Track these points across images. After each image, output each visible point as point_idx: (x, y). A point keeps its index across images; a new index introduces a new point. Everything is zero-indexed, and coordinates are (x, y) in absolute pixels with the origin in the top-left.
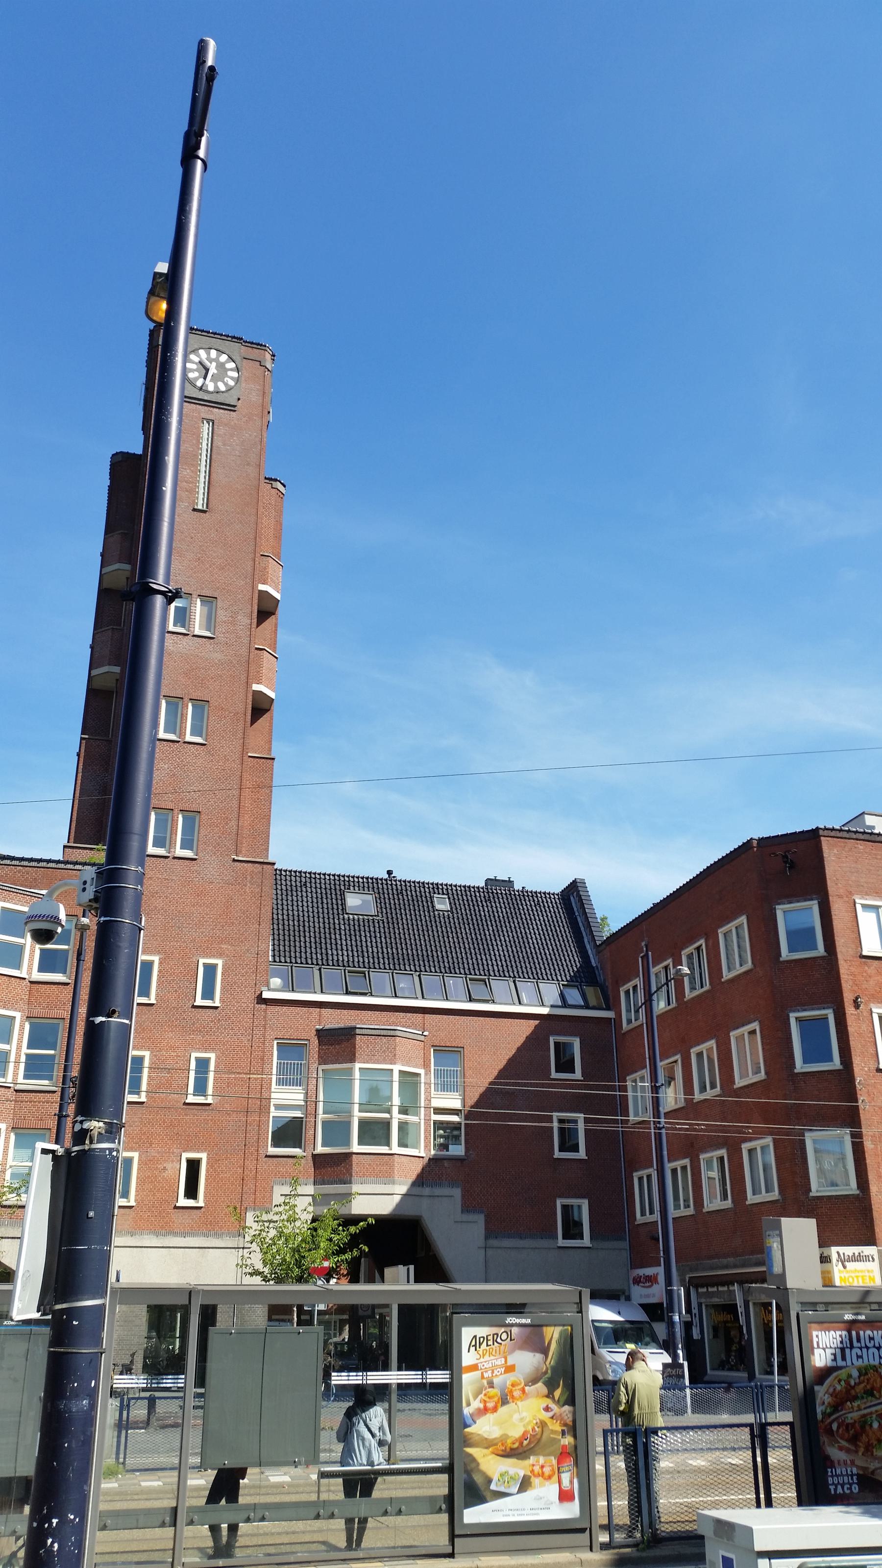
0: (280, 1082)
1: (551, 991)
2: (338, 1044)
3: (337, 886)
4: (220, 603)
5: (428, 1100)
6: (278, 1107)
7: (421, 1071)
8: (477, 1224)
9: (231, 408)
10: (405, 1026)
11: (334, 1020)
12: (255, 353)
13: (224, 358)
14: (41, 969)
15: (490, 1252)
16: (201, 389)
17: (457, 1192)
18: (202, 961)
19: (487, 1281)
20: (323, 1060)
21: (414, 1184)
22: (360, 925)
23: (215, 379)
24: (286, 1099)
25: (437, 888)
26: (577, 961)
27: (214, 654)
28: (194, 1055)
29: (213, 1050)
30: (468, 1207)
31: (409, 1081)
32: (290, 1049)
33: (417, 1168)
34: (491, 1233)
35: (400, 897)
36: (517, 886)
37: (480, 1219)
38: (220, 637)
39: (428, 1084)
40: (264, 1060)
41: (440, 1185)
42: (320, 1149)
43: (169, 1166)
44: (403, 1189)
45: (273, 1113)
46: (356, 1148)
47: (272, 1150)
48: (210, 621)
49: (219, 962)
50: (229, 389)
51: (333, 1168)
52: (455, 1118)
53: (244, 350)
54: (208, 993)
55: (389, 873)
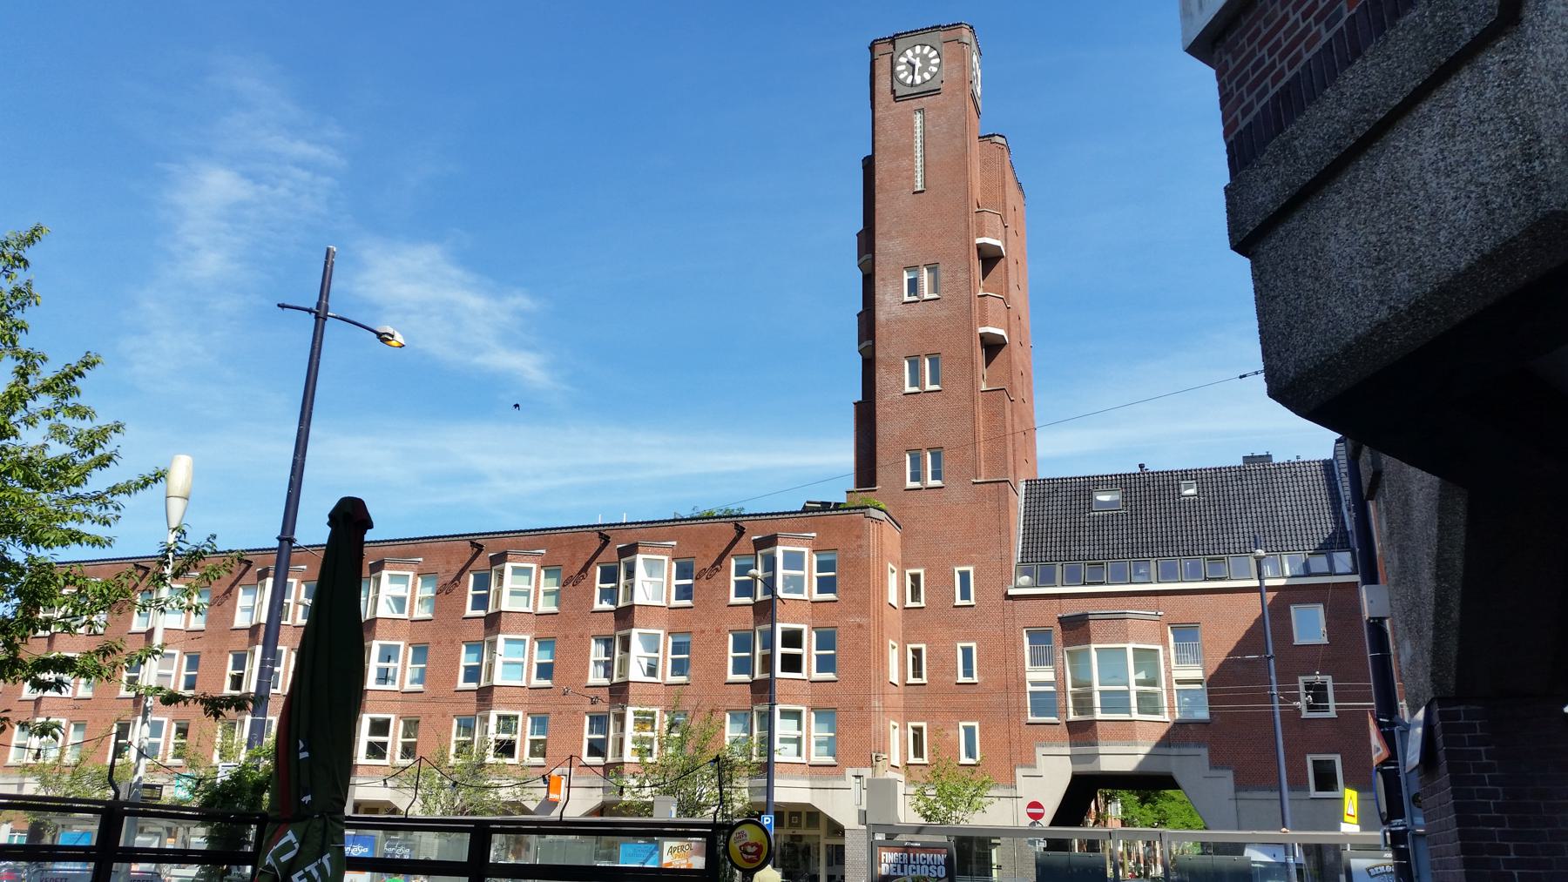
0: (1033, 663)
1: (265, 808)
2: (1076, 628)
3: (1085, 487)
4: (941, 267)
5: (1169, 672)
6: (1033, 684)
7: (1160, 648)
8: (1227, 779)
9: (936, 92)
10: (1133, 609)
11: (1072, 608)
12: (953, 34)
13: (918, 49)
14: (820, 592)
15: (1240, 803)
16: (912, 85)
17: (1204, 752)
18: (957, 569)
19: (1239, 829)
20: (1066, 643)
21: (1158, 745)
22: (1110, 519)
23: (921, 71)
24: (1038, 676)
25: (1185, 474)
26: (1330, 527)
27: (940, 312)
28: (959, 645)
29: (974, 640)
30: (1215, 764)
31: (1145, 658)
32: (1039, 636)
33: (1163, 730)
34: (1240, 785)
35: (1149, 490)
36: (1275, 460)
37: (1229, 774)
38: (946, 297)
39: (1167, 659)
40: (1017, 645)
41: (1187, 746)
42: (1072, 717)
43: (950, 732)
44: (1147, 750)
45: (1029, 688)
46: (1099, 715)
47: (1031, 719)
48: (935, 287)
49: (971, 569)
50: (934, 75)
51: (1082, 732)
52: (1199, 686)
53: (942, 35)
54: (965, 594)
55: (1141, 466)
